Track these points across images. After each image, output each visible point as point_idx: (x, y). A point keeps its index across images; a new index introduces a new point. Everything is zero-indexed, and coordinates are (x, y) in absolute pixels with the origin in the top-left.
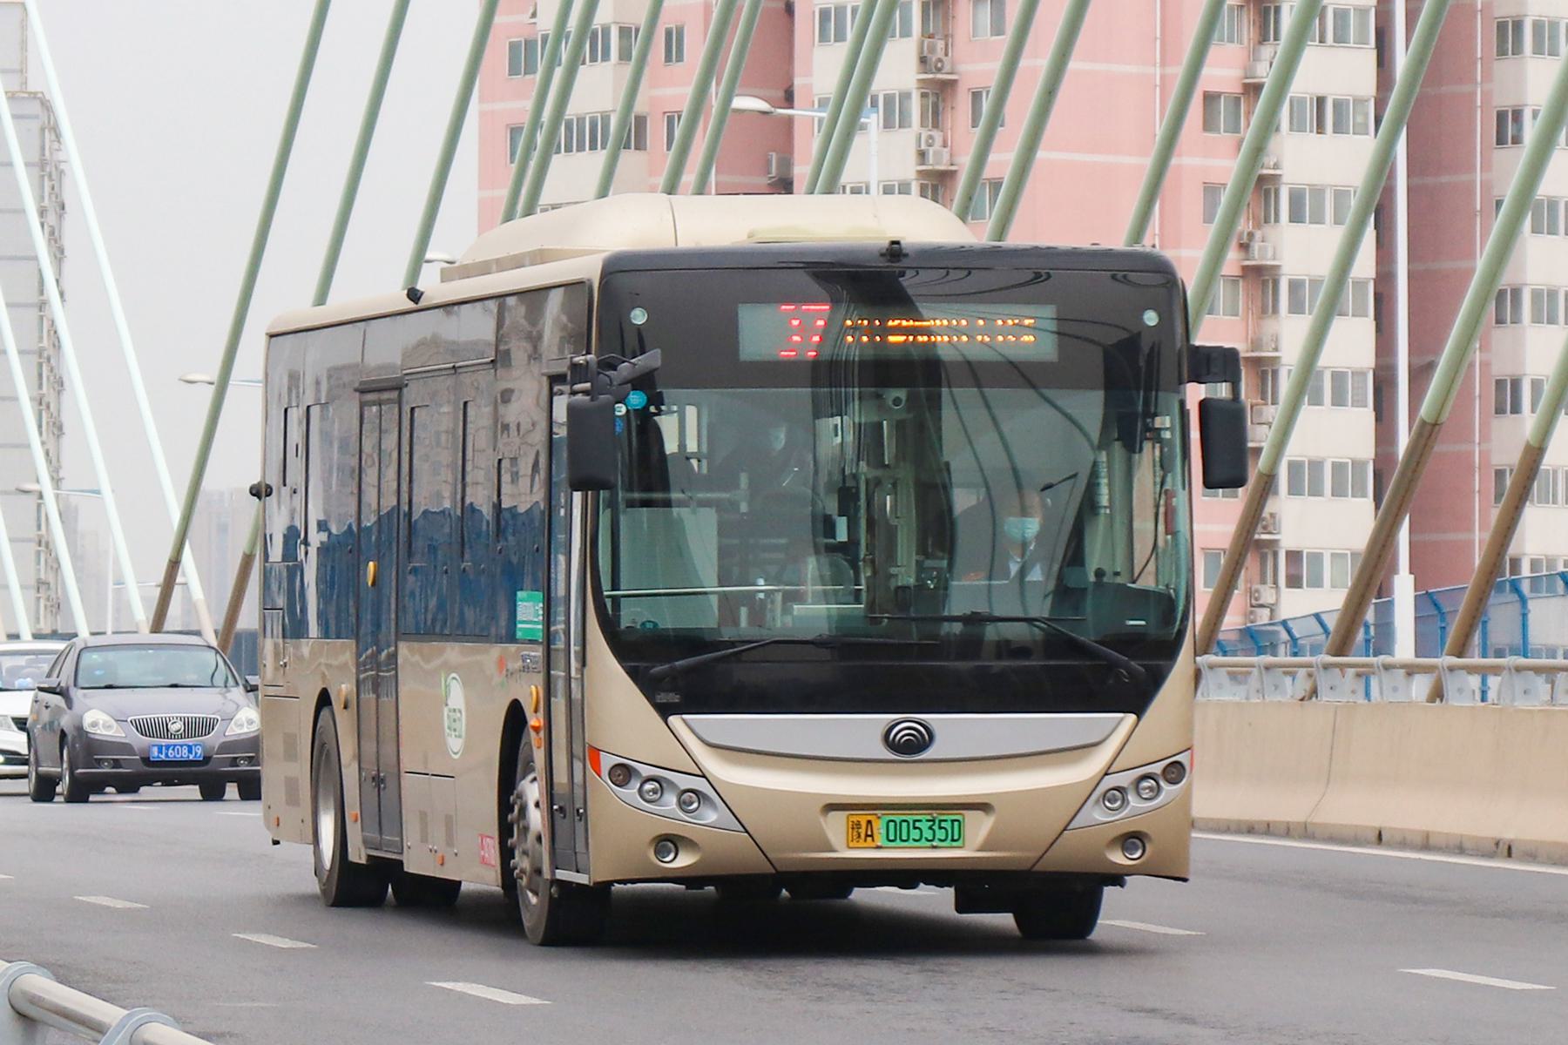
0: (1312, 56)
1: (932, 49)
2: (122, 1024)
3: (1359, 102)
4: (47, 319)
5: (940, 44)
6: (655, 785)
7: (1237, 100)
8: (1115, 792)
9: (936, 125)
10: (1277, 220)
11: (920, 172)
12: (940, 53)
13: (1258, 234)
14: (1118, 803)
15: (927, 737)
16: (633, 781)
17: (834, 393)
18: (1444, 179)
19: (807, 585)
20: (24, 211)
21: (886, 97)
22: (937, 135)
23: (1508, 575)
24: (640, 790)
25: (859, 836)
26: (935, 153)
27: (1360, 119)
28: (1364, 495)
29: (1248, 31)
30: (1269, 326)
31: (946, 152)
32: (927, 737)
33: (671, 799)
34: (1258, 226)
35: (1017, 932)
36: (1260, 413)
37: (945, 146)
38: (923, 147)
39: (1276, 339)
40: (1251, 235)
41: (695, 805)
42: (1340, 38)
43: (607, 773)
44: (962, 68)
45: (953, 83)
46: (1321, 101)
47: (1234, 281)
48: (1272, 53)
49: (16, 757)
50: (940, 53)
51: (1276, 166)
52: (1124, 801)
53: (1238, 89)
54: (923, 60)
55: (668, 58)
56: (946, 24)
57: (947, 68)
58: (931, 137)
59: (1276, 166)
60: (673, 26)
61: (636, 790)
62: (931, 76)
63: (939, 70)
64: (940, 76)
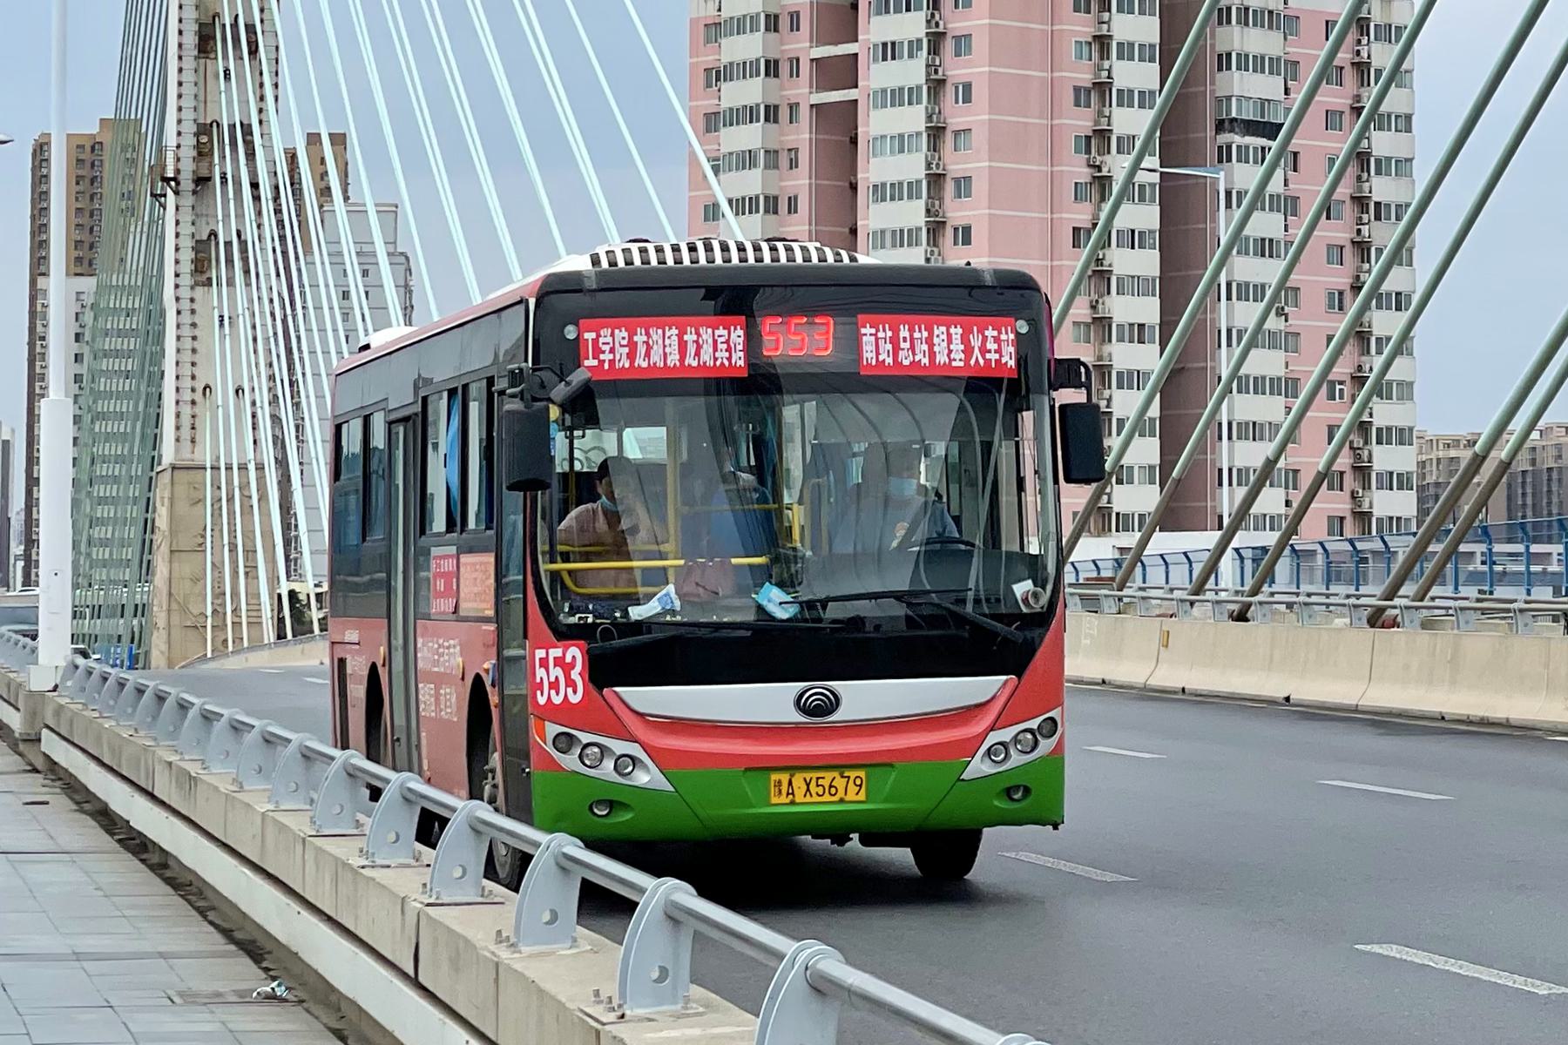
0: (1125, 208)
1: (933, 205)
2: (463, 809)
3: (1151, 232)
4: (1450, 466)
5: (937, 203)
6: (596, 750)
7: (1090, 91)
8: (999, 746)
9: (935, 245)
10: (1110, 341)
11: (927, 33)
12: (937, 208)
13: (1100, 301)
14: (1002, 756)
15: (831, 697)
16: (573, 750)
17: (1529, 512)
18: (1190, 273)
19: (636, 586)
20: (386, 308)
21: (908, 230)
22: (936, 250)
23: (516, 272)
24: (581, 757)
25: (780, 791)
26: (935, 259)
27: (1151, 241)
28: (1155, 436)
29: (1095, 196)
30: (1107, 348)
31: (940, 258)
32: (831, 697)
33: (609, 764)
34: (1101, 296)
35: (916, 870)
36: (1102, 393)
37: (939, 255)
38: (929, 256)
39: (1110, 354)
40: (1097, 301)
41: (630, 768)
42: (1142, 199)
43: (551, 742)
44: (948, 215)
45: (944, 223)
46: (1133, 231)
47: (1090, 277)
48: (1107, 207)
49: (980, 469)
50: (937, 208)
51: (1110, 265)
52: (1007, 756)
53: (1090, 85)
54: (928, 211)
55: (789, 212)
56: (939, 191)
57: (941, 215)
58: (932, 251)
59: (1110, 265)
60: (792, 195)
61: (577, 756)
62: (932, 219)
63: (937, 216)
64: (937, 219)
